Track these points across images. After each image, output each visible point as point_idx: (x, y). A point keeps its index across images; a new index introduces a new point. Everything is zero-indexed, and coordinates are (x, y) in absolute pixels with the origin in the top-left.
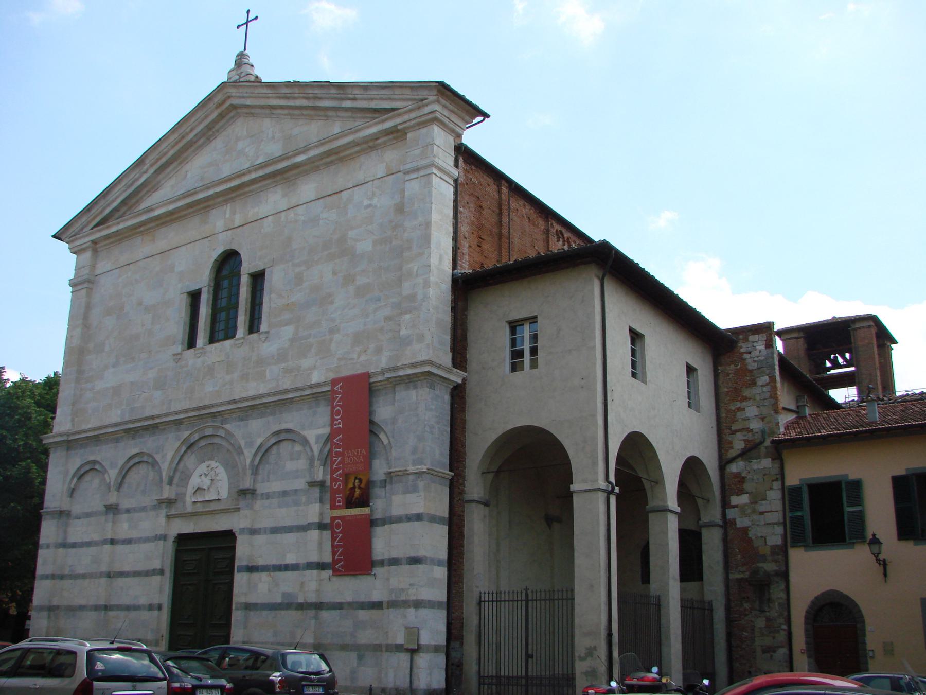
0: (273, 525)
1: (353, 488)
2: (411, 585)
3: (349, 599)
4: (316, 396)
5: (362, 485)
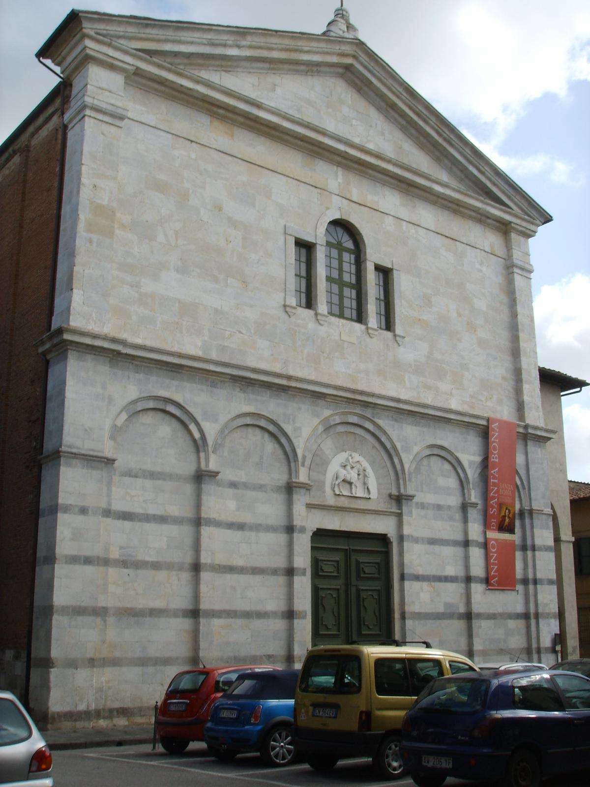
1: (504, 517)
2: (551, 601)
3: (500, 610)
5: (510, 516)
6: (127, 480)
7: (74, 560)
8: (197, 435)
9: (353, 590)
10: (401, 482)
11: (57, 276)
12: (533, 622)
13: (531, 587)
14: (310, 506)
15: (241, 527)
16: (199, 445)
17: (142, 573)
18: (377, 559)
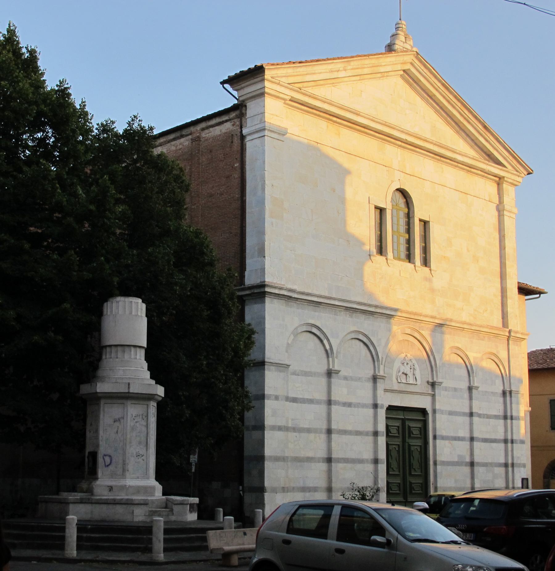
6: (294, 377)
7: (273, 428)
8: (328, 347)
9: (407, 444)
10: (434, 372)
11: (247, 243)
12: (510, 469)
13: (509, 445)
14: (386, 390)
15: (350, 405)
16: (328, 353)
17: (303, 435)
18: (419, 425)
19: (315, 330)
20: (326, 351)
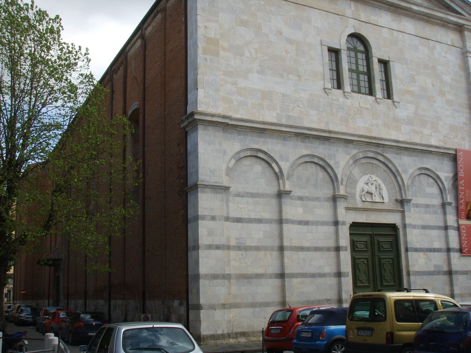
0: (423, 224)
4: (443, 154)
6: (238, 199)
7: (210, 247)
8: (277, 170)
9: (377, 258)
10: (403, 191)
14: (347, 209)
15: (306, 223)
16: (279, 176)
19: (261, 155)
20: (276, 173)
